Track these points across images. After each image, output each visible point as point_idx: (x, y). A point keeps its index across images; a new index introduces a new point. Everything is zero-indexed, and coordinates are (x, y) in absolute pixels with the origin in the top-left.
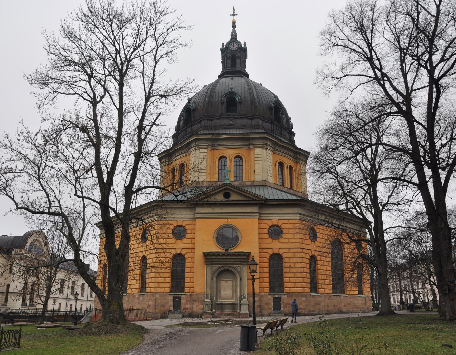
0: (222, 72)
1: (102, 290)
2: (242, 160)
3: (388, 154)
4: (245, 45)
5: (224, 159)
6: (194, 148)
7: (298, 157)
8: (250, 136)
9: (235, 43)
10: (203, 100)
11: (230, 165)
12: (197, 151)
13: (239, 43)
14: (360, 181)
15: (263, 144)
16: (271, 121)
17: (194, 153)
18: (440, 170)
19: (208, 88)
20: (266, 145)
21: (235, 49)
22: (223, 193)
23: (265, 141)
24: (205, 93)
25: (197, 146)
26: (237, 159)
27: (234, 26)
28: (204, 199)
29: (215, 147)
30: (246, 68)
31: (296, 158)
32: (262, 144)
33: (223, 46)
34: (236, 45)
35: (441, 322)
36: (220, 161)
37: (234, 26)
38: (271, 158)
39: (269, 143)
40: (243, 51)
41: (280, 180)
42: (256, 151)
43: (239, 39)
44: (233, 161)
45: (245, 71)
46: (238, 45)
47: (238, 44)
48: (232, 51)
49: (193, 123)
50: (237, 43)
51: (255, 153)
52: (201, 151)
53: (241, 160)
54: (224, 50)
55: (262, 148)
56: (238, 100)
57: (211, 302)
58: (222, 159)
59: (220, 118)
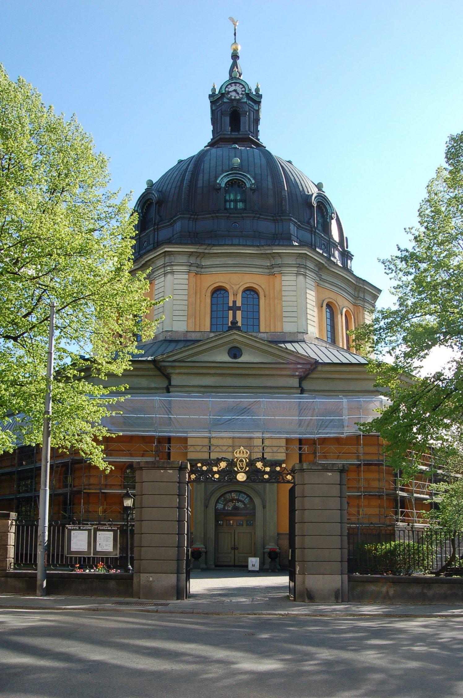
0: (212, 139)
1: (447, 253)
2: (258, 295)
3: (451, 339)
4: (257, 90)
5: (223, 292)
6: (163, 270)
7: (361, 295)
12: (169, 276)
13: (244, 85)
15: (299, 266)
16: (315, 232)
17: (163, 279)
18: (245, 479)
19: (185, 167)
20: (305, 267)
23: (303, 262)
25: (168, 266)
26: (248, 292)
28: (189, 358)
29: (203, 270)
31: (356, 298)
32: (298, 267)
33: (214, 89)
34: (239, 88)
36: (215, 295)
39: (310, 265)
41: (329, 333)
42: (284, 278)
46: (243, 89)
47: (244, 87)
48: (232, 100)
49: (158, 225)
50: (241, 86)
51: (284, 283)
53: (256, 296)
55: (298, 274)
56: (248, 186)
57: (206, 548)
58: (218, 293)
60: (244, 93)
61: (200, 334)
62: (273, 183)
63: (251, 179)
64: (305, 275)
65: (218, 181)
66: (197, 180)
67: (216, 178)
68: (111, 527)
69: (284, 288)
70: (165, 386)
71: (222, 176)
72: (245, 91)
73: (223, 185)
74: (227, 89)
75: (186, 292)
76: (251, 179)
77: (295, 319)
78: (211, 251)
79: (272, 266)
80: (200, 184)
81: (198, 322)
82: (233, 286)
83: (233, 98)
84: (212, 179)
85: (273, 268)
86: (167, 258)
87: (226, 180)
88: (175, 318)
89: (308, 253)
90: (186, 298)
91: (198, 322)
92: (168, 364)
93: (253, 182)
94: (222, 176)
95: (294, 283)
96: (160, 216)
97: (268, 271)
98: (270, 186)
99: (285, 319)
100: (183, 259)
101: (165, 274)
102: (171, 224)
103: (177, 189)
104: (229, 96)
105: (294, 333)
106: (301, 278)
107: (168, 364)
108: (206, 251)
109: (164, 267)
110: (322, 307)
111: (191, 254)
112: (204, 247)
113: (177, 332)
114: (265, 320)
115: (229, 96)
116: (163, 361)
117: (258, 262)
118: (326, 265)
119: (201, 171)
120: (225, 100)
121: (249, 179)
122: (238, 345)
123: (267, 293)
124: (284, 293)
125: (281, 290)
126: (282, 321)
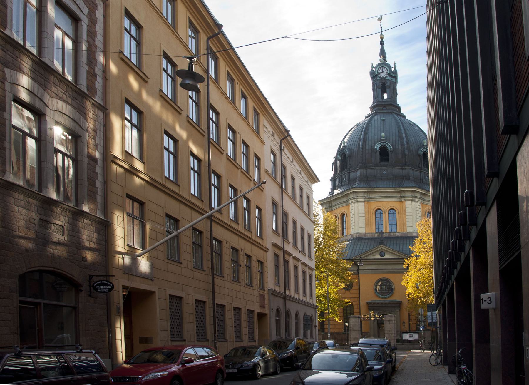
0: (374, 103)
8: (401, 190)
9: (384, 68)
10: (357, 151)
11: (385, 218)
12: (356, 204)
13: (389, 66)
14: (363, 320)
15: (412, 197)
16: (422, 171)
19: (359, 134)
20: (416, 197)
21: (384, 77)
22: (379, 252)
24: (356, 142)
25: (355, 198)
27: (382, 43)
29: (371, 200)
30: (397, 95)
35: (345, 315)
36: (377, 213)
37: (382, 43)
38: (420, 207)
40: (393, 75)
42: (406, 203)
43: (388, 62)
44: (387, 213)
45: (396, 103)
46: (387, 71)
51: (406, 206)
52: (359, 204)
54: (374, 75)
55: (412, 201)
56: (389, 149)
59: (373, 168)
60: (387, 73)
61: (371, 234)
62: (401, 145)
63: (390, 146)
64: (415, 201)
65: (375, 148)
66: (366, 145)
67: (374, 146)
68: (316, 326)
69: (407, 209)
70: (357, 269)
71: (377, 144)
72: (388, 72)
73: (378, 149)
74: (378, 71)
75: (364, 212)
76: (390, 146)
77: (411, 225)
78: (374, 190)
79: (401, 197)
80: (367, 148)
81: (370, 228)
82: (384, 208)
83: (382, 77)
84: (373, 145)
85: (401, 198)
86: (355, 194)
87: (379, 146)
88: (360, 226)
89: (416, 190)
90: (364, 215)
91: (370, 228)
92: (357, 260)
93: (391, 147)
94: (377, 144)
95: (410, 206)
96: (350, 164)
97: (399, 199)
98: (400, 148)
99: (407, 225)
100: (361, 195)
101: (354, 202)
102: (355, 171)
103: (357, 149)
104: (380, 76)
105: (411, 232)
106: (414, 203)
107: (357, 260)
108: (372, 191)
109: (354, 199)
110: (425, 215)
111: (365, 192)
112: (371, 189)
113: (361, 233)
114: (399, 225)
115: (380, 76)
116: (355, 259)
117: (395, 195)
118: (426, 193)
119: (367, 139)
120: (378, 78)
121: (389, 146)
122: (383, 251)
123: (399, 211)
124: (407, 212)
125: (405, 209)
126: (406, 227)
